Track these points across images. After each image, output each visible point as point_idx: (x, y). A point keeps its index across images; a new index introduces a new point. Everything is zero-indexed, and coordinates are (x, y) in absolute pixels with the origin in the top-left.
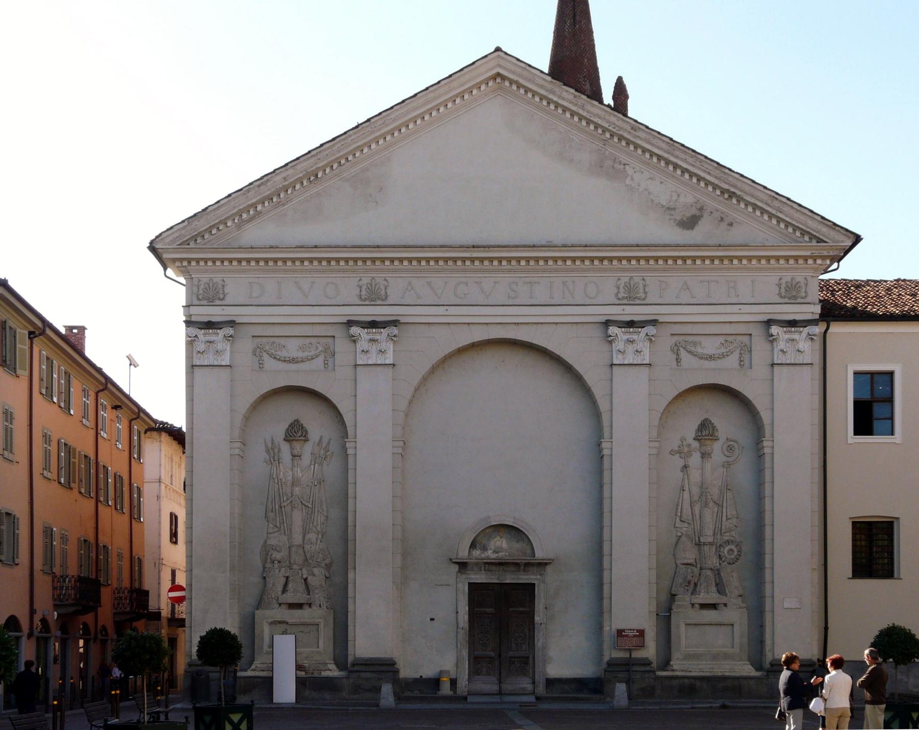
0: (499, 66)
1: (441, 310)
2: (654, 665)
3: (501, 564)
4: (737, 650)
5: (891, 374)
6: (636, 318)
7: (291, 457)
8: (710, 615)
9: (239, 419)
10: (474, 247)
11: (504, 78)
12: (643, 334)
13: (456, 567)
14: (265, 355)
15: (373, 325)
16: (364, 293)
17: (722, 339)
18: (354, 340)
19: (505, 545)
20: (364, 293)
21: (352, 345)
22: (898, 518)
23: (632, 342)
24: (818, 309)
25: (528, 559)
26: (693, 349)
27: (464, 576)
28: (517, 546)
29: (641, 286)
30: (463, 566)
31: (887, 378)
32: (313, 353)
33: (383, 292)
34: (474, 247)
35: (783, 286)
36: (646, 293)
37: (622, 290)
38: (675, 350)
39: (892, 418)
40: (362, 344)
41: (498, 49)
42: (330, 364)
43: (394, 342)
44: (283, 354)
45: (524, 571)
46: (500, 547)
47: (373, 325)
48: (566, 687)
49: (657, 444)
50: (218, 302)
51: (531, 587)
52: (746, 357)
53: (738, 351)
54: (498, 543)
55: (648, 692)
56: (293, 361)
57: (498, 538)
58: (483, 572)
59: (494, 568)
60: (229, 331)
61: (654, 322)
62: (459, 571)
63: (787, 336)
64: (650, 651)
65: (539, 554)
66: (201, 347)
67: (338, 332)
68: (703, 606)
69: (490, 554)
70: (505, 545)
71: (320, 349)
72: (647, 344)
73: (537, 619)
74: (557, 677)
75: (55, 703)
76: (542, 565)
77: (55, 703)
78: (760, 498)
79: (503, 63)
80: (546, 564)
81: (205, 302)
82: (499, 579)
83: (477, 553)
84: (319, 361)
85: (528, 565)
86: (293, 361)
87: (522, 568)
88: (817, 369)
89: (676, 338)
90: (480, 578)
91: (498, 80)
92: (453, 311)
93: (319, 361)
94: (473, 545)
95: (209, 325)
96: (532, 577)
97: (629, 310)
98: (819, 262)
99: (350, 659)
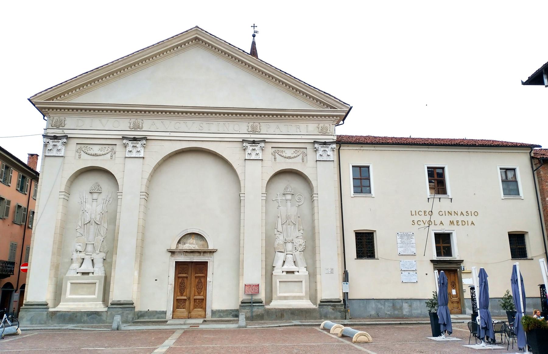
0: (197, 34)
1: (167, 134)
2: (264, 302)
3: (192, 252)
4: (303, 294)
5: (368, 167)
6: (327, 141)
7: (91, 200)
8: (290, 277)
9: (145, 181)
11: (199, 39)
12: (330, 148)
13: (170, 254)
14: (82, 152)
15: (135, 139)
16: (132, 125)
17: (294, 150)
18: (316, 150)
20: (132, 125)
21: (124, 148)
22: (375, 231)
23: (254, 150)
24: (335, 138)
25: (205, 249)
26: (281, 154)
28: (201, 243)
29: (258, 127)
30: (173, 253)
31: (367, 169)
32: (106, 152)
33: (141, 126)
34: (143, 240)
35: (320, 128)
36: (260, 129)
37: (250, 128)
38: (273, 154)
39: (370, 186)
40: (130, 148)
41: (197, 27)
42: (305, 160)
43: (145, 147)
44: (284, 154)
46: (192, 244)
47: (135, 139)
48: (222, 314)
49: (265, 195)
50: (61, 128)
51: (205, 264)
52: (305, 158)
53: (301, 155)
55: (261, 317)
56: (96, 155)
60: (144, 142)
61: (264, 141)
63: (322, 149)
64: (262, 296)
65: (211, 247)
66: (50, 147)
67: (309, 146)
68: (288, 272)
71: (109, 150)
72: (143, 149)
76: (212, 252)
78: (313, 221)
79: (198, 32)
80: (214, 252)
81: (55, 128)
84: (109, 156)
85: (205, 252)
86: (96, 155)
88: (336, 162)
89: (79, 146)
90: (182, 258)
91: (197, 40)
92: (172, 134)
93: (109, 156)
94: (179, 242)
95: (55, 138)
97: (253, 136)
98: (335, 118)
99: (110, 302)
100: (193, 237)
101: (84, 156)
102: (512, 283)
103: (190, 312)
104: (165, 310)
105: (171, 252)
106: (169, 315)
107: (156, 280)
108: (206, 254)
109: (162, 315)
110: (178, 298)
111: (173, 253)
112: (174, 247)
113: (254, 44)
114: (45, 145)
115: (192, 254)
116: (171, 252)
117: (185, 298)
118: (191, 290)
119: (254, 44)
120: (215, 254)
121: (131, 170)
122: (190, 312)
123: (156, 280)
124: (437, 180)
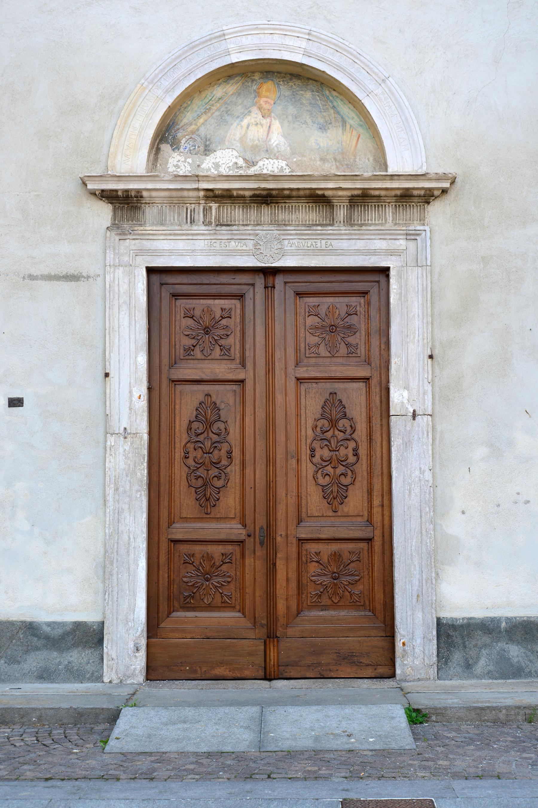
10: (370, 422)
13: (104, 212)
19: (277, 139)
27: (130, 244)
30: (125, 203)
34: (370, 422)
45: (349, 221)
46: (263, 140)
48: (515, 652)
54: (256, 134)
57: (255, 115)
58: (200, 228)
59: (237, 213)
62: (115, 226)
65: (404, 159)
69: (223, 163)
70: (277, 139)
73: (398, 396)
74: (478, 613)
75: (188, 668)
76: (414, 197)
77: (188, 668)
80: (428, 197)
82: (256, 252)
83: (177, 162)
85: (362, 199)
87: (341, 213)
94: (166, 134)
96: (380, 244)
100: (269, 90)
102: (75, 623)
103: (271, 636)
104: (89, 616)
105: (108, 196)
106: (126, 650)
107: (15, 403)
108: (371, 215)
109: (76, 657)
110: (180, 531)
111: (125, 203)
112: (129, 160)
115: (266, 212)
116: (108, 196)
117: (234, 529)
118: (16, 402)
120: (436, 209)
122: (271, 636)
123: (15, 403)
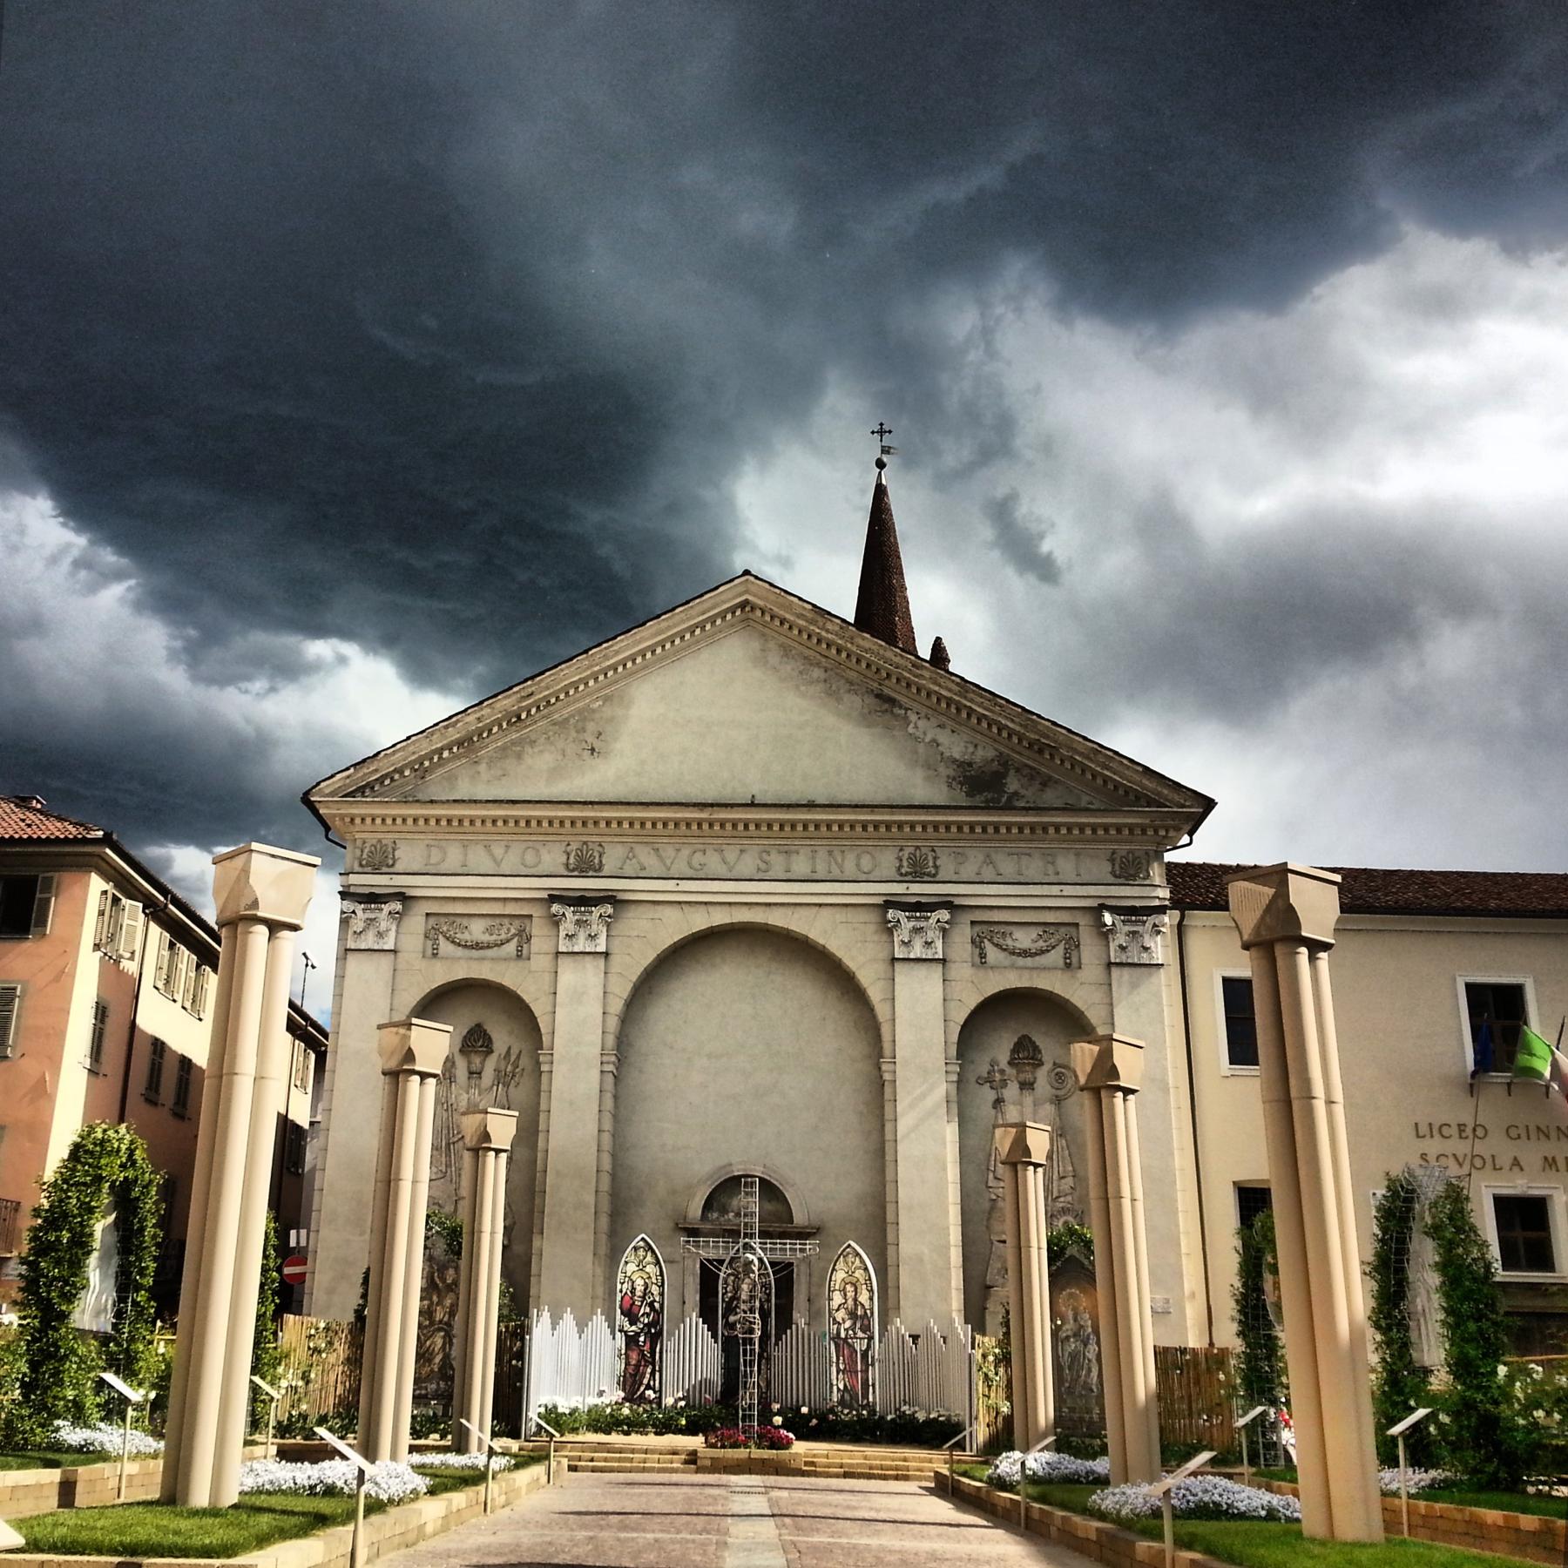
38: (977, 943)
56: (477, 946)
86: (1025, 953)
101: (445, 947)
113: (880, 491)
114: (345, 922)
119: (880, 491)
121: (576, 1004)
124: (1497, 1016)
